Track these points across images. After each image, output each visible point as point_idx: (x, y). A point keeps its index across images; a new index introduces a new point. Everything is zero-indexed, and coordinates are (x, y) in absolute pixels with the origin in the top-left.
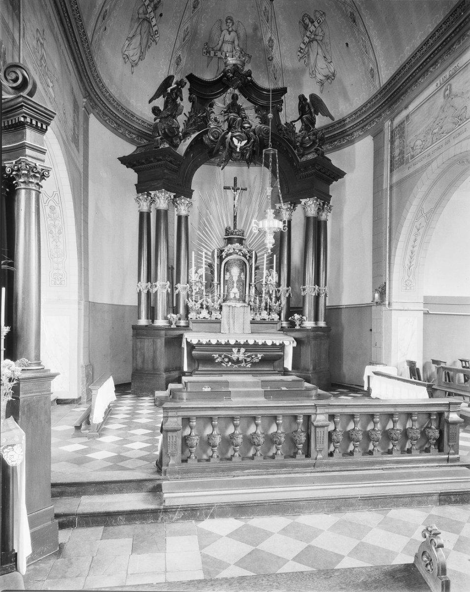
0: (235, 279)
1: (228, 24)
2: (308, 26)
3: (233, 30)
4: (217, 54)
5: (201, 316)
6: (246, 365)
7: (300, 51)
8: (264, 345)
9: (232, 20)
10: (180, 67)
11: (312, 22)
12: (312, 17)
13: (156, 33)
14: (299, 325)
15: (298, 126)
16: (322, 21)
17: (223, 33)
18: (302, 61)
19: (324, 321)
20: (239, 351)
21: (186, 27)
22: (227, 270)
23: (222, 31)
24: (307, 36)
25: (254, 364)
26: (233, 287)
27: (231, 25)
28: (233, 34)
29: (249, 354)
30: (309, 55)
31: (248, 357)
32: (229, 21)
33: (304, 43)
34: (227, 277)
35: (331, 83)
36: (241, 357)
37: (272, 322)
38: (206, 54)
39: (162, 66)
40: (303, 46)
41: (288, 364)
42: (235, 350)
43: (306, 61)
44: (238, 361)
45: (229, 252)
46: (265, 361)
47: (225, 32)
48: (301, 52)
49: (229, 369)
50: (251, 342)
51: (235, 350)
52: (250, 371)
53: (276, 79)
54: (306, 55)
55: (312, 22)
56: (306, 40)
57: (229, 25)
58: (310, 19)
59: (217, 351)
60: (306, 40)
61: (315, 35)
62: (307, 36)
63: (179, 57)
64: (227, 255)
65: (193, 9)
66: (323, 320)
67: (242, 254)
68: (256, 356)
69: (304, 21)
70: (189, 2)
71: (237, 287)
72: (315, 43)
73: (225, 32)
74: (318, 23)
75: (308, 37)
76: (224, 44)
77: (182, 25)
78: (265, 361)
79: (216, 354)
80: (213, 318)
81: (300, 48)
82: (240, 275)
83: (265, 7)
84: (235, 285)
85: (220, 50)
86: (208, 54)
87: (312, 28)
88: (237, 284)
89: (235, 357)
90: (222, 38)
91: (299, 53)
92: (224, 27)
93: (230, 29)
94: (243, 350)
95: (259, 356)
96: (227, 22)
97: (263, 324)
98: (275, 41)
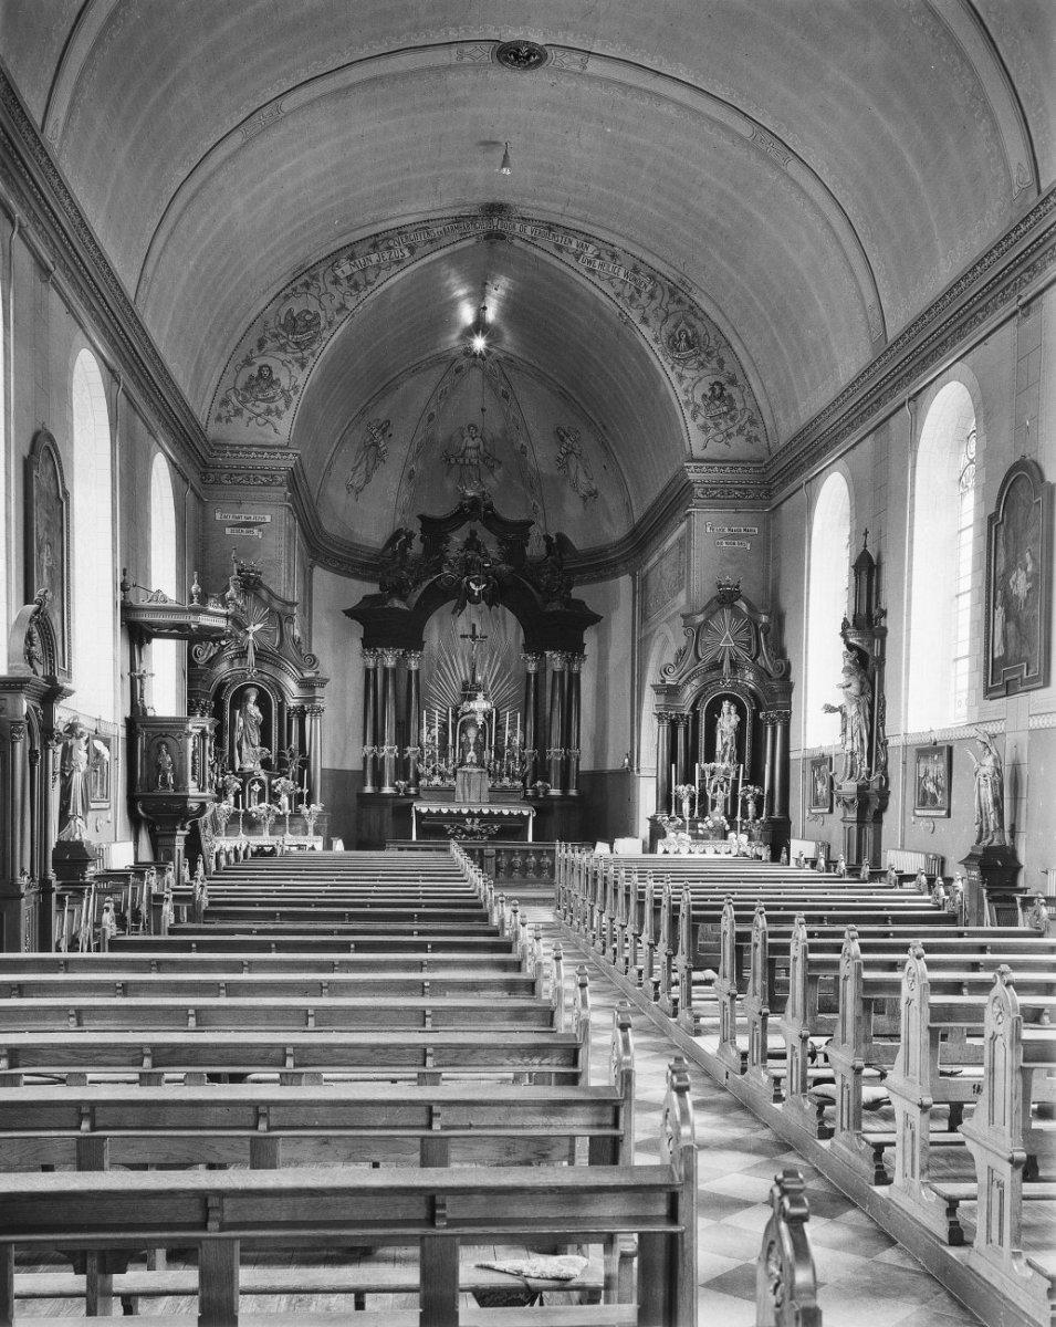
0: (472, 741)
22: (463, 731)
42: (468, 821)
51: (468, 821)
60: (564, 451)
89: (468, 827)
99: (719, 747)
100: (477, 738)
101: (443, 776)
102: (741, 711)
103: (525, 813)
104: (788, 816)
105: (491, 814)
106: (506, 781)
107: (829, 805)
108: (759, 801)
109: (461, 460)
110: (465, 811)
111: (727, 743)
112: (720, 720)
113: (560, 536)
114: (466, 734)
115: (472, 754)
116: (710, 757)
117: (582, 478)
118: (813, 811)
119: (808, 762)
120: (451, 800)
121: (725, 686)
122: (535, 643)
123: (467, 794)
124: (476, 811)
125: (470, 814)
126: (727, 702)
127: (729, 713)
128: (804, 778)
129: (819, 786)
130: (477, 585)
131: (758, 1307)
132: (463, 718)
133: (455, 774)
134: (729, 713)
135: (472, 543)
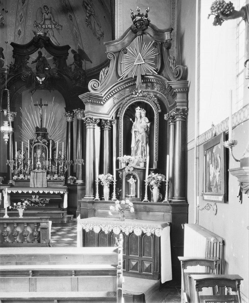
0: (39, 156)
1: (45, 9)
2: (86, 7)
3: (49, 13)
4: (42, 26)
5: (20, 178)
6: (42, 205)
7: (86, 21)
8: (49, 193)
9: (47, 7)
10: (21, 36)
11: (88, 5)
12: (87, 2)
13: (2, 19)
14: (73, 182)
15: (73, 67)
16: (92, 4)
17: (44, 14)
18: (89, 26)
19: (82, 180)
20: (36, 197)
21: (20, 14)
22: (35, 152)
23: (43, 14)
24: (87, 13)
25: (47, 205)
26: (38, 161)
27: (47, 9)
28: (49, 14)
29: (42, 199)
30: (91, 23)
31: (41, 200)
32: (45, 8)
33: (87, 16)
34: (35, 155)
35: (103, 39)
36: (37, 200)
37: (60, 181)
38: (36, 27)
39: (9, 37)
40: (87, 18)
41: (65, 205)
42: (34, 197)
43: (90, 26)
44: (36, 203)
45: (35, 141)
46: (52, 203)
47: (44, 14)
48: (87, 22)
49: (33, 207)
50: (41, 192)
51: (34, 197)
52: (45, 208)
53: (77, 38)
54: (90, 23)
55: (88, 5)
56: (88, 15)
57: (46, 10)
58: (86, 3)
59: (24, 197)
60: (88, 15)
61: (91, 12)
62: (87, 13)
63: (20, 30)
64: (35, 143)
65: (23, 4)
66: (81, 179)
67: (42, 142)
68: (46, 200)
69: (84, 5)
70: (19, 1)
71: (40, 161)
72: (92, 16)
73: (44, 14)
74: (91, 5)
75: (88, 13)
76: (45, 21)
77: (18, 13)
78: (52, 203)
79: (23, 199)
80: (26, 179)
81: (86, 19)
82: (42, 154)
83: (22, 14)
84: (39, 160)
85: (44, 24)
86: (37, 27)
87: (89, 8)
88: (40, 160)
89: (33, 200)
90: (43, 17)
91: (86, 22)
92: (44, 11)
93: (47, 12)
94: (38, 197)
95: (47, 200)
96: (44, 9)
97: (56, 182)
98: (73, 16)
99: (133, 145)
100: (41, 155)
101: (25, 174)
102: (150, 115)
103: (62, 192)
104: (187, 201)
105: (54, 193)
106: (56, 176)
107: (222, 191)
108: (162, 190)
109: (44, 26)
110: (30, 192)
111: (139, 140)
112: (134, 123)
113: (80, 50)
114: (36, 153)
115: (39, 163)
116: (128, 151)
117: (97, 28)
118: (206, 197)
119: (202, 147)
120: (28, 187)
121: (138, 96)
122: (69, 109)
123: (35, 184)
124: (36, 192)
125: (33, 193)
126: (139, 108)
127: (141, 117)
128: (198, 165)
129: (212, 169)
130: (41, 78)
131: (221, 201)
132: (34, 145)
133: (30, 174)
134: (141, 117)
135: (41, 61)
